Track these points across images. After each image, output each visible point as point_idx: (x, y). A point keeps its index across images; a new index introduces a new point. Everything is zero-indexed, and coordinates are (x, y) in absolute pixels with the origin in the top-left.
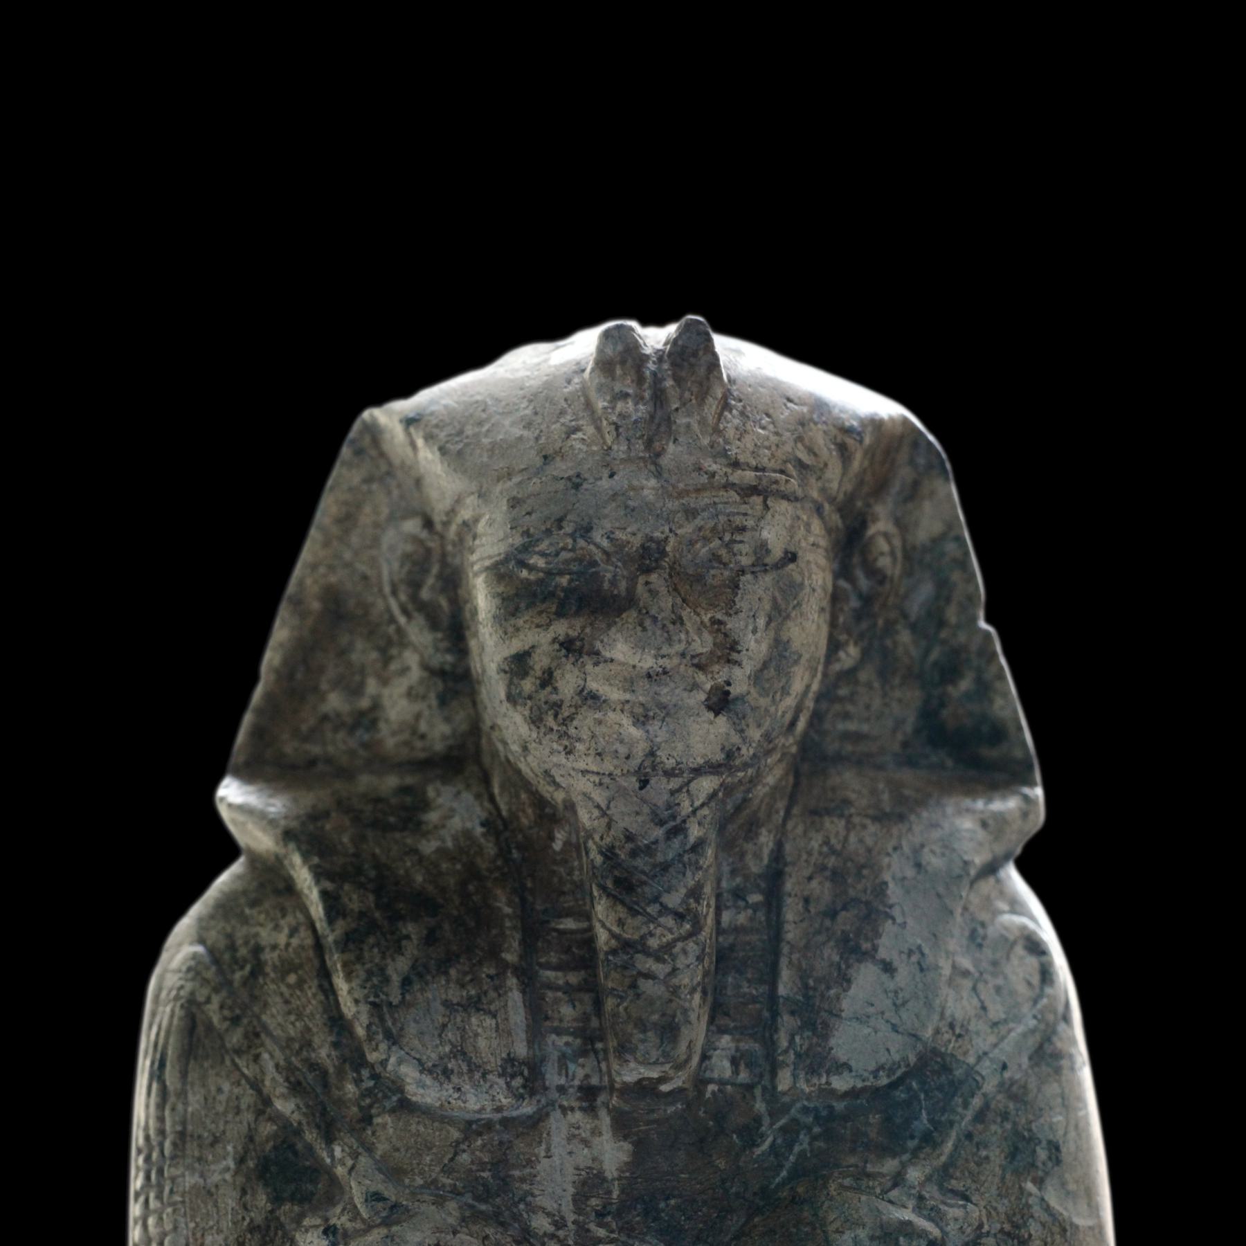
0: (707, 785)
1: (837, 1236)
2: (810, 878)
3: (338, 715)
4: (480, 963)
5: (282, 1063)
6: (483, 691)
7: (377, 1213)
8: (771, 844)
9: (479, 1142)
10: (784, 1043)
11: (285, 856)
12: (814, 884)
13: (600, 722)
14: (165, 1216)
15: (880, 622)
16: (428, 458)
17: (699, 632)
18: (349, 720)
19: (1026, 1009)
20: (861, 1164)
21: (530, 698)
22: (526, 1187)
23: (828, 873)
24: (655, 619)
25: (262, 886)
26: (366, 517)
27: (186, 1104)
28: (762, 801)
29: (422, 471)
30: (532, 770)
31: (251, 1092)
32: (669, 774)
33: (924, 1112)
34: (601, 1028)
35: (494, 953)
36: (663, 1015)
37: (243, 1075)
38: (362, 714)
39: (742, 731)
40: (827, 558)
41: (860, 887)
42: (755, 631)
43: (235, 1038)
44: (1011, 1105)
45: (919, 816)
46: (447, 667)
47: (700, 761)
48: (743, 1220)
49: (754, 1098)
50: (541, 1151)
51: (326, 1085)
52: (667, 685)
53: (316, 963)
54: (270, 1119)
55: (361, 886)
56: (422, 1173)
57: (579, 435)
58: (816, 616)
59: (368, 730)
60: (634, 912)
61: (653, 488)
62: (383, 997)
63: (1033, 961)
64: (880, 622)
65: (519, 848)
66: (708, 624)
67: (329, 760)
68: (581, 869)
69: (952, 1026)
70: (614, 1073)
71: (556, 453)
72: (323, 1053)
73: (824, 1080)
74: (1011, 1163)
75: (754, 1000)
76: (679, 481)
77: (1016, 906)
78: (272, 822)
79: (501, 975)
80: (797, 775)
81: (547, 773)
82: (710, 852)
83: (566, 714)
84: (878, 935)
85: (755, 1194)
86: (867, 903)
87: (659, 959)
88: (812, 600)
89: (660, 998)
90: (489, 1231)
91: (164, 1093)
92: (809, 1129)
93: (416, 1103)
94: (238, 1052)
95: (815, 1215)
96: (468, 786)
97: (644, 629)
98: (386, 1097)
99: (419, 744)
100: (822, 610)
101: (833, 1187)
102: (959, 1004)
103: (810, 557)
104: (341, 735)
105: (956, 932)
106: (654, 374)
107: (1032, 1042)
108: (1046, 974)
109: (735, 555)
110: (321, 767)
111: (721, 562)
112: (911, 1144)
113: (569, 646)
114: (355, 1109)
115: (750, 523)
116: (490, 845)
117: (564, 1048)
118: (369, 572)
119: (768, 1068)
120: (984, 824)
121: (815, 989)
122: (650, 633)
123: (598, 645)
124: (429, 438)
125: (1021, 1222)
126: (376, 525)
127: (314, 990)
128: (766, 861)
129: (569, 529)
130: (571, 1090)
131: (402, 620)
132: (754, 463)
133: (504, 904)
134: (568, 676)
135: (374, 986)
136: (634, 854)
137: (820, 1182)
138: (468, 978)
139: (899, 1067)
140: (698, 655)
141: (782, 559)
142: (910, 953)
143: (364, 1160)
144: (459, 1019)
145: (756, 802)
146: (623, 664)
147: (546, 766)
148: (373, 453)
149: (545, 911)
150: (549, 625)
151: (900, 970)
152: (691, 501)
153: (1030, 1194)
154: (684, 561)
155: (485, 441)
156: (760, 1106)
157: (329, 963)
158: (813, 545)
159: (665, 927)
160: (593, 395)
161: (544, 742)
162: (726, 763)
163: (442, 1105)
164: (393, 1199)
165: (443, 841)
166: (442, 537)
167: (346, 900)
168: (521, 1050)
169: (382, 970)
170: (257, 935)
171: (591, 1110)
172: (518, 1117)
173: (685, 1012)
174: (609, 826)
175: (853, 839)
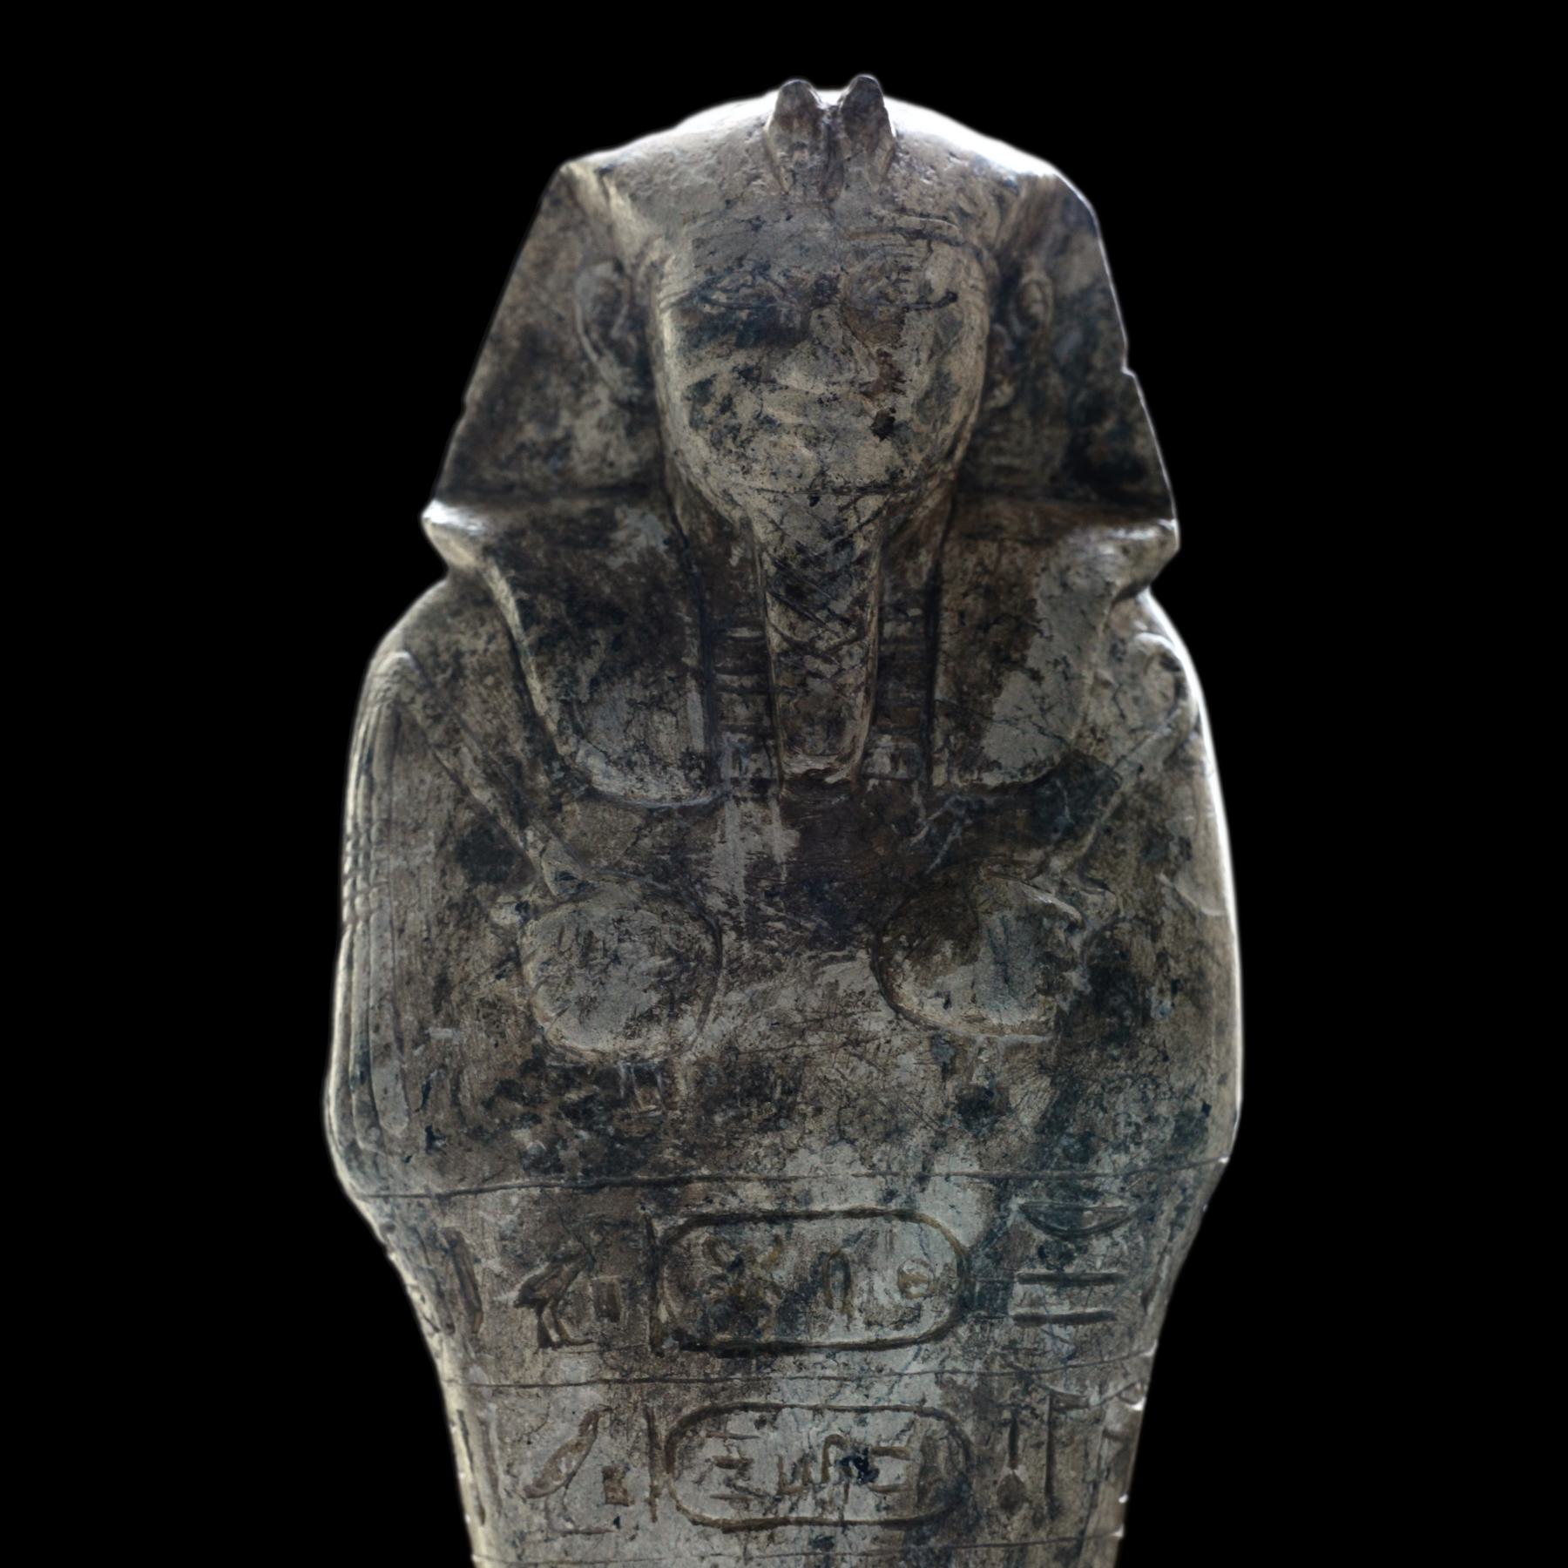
0: (872, 503)
1: (986, 916)
2: (965, 595)
3: (534, 444)
4: (662, 667)
5: (480, 757)
6: (668, 418)
7: (565, 891)
8: (930, 564)
9: (659, 829)
10: (939, 743)
11: (485, 570)
12: (969, 600)
13: (775, 445)
14: (370, 896)
15: (1033, 365)
16: (619, 205)
17: (867, 362)
18: (544, 450)
19: (1161, 718)
20: (1008, 853)
21: (711, 422)
22: (702, 869)
23: (981, 591)
24: (826, 349)
25: (463, 597)
26: (562, 262)
27: (391, 794)
28: (922, 522)
29: (614, 217)
30: (711, 490)
31: (451, 782)
32: (838, 492)
33: (1067, 810)
34: (773, 727)
35: (675, 658)
36: (830, 710)
37: (445, 768)
38: (556, 443)
39: (905, 455)
40: (985, 300)
41: (1011, 603)
42: (918, 363)
43: (437, 735)
44: (1147, 805)
45: (1066, 543)
46: (635, 400)
47: (867, 481)
48: (900, 902)
49: (912, 793)
50: (716, 837)
51: (520, 776)
52: (837, 410)
53: (512, 666)
54: (469, 807)
55: (553, 596)
56: (607, 855)
57: (759, 182)
58: (974, 353)
59: (561, 458)
60: (803, 617)
61: (826, 231)
62: (574, 696)
63: (1167, 676)
64: (1033, 365)
65: (698, 563)
66: (875, 355)
67: (525, 486)
68: (755, 582)
69: (1093, 731)
70: (784, 765)
71: (737, 198)
72: (518, 747)
73: (975, 777)
74: (1146, 856)
75: (912, 703)
76: (849, 224)
77: (1152, 627)
78: (473, 539)
80: (954, 503)
81: (725, 492)
82: (874, 565)
83: (744, 437)
84: (1027, 646)
85: (911, 878)
86: (1017, 618)
87: (827, 660)
88: (971, 338)
89: (827, 695)
91: (371, 786)
92: (962, 821)
93: (602, 792)
94: (439, 746)
95: (966, 897)
96: (652, 509)
97: (817, 358)
98: (575, 787)
99: (607, 471)
100: (980, 347)
101: (982, 872)
102: (1101, 712)
103: (970, 298)
104: (536, 463)
105: (1099, 646)
106: (829, 127)
107: (1167, 748)
108: (1180, 689)
109: (901, 293)
110: (517, 492)
111: (888, 300)
112: (1055, 837)
113: (748, 376)
114: (546, 798)
115: (915, 264)
116: (672, 561)
118: (563, 313)
119: (924, 765)
120: (1125, 551)
121: (968, 694)
122: (822, 362)
123: (774, 374)
124: (621, 186)
125: (1154, 909)
126: (571, 270)
127: (510, 691)
128: (925, 578)
129: (748, 266)
130: (744, 783)
131: (594, 357)
132: (919, 209)
133: (684, 614)
134: (746, 402)
135: (565, 686)
136: (805, 564)
137: (972, 868)
138: (651, 679)
139: (1045, 766)
140: (866, 384)
141: (944, 298)
142: (1056, 663)
143: (554, 844)
144: (642, 716)
145: (917, 524)
146: (797, 391)
147: (725, 486)
148: (569, 203)
149: (723, 621)
150: (729, 355)
151: (1047, 678)
152: (861, 242)
153: (1163, 885)
154: (854, 298)
155: (673, 188)
156: (917, 800)
157: (524, 666)
158: (973, 287)
159: (833, 632)
160: (772, 145)
161: (724, 463)
162: (889, 484)
163: (625, 795)
164: (580, 878)
165: (630, 557)
166: (631, 280)
167: (539, 608)
168: (699, 745)
169: (572, 672)
170: (457, 642)
171: (762, 801)
172: (695, 806)
173: (850, 708)
174: (782, 539)
175: (1005, 560)
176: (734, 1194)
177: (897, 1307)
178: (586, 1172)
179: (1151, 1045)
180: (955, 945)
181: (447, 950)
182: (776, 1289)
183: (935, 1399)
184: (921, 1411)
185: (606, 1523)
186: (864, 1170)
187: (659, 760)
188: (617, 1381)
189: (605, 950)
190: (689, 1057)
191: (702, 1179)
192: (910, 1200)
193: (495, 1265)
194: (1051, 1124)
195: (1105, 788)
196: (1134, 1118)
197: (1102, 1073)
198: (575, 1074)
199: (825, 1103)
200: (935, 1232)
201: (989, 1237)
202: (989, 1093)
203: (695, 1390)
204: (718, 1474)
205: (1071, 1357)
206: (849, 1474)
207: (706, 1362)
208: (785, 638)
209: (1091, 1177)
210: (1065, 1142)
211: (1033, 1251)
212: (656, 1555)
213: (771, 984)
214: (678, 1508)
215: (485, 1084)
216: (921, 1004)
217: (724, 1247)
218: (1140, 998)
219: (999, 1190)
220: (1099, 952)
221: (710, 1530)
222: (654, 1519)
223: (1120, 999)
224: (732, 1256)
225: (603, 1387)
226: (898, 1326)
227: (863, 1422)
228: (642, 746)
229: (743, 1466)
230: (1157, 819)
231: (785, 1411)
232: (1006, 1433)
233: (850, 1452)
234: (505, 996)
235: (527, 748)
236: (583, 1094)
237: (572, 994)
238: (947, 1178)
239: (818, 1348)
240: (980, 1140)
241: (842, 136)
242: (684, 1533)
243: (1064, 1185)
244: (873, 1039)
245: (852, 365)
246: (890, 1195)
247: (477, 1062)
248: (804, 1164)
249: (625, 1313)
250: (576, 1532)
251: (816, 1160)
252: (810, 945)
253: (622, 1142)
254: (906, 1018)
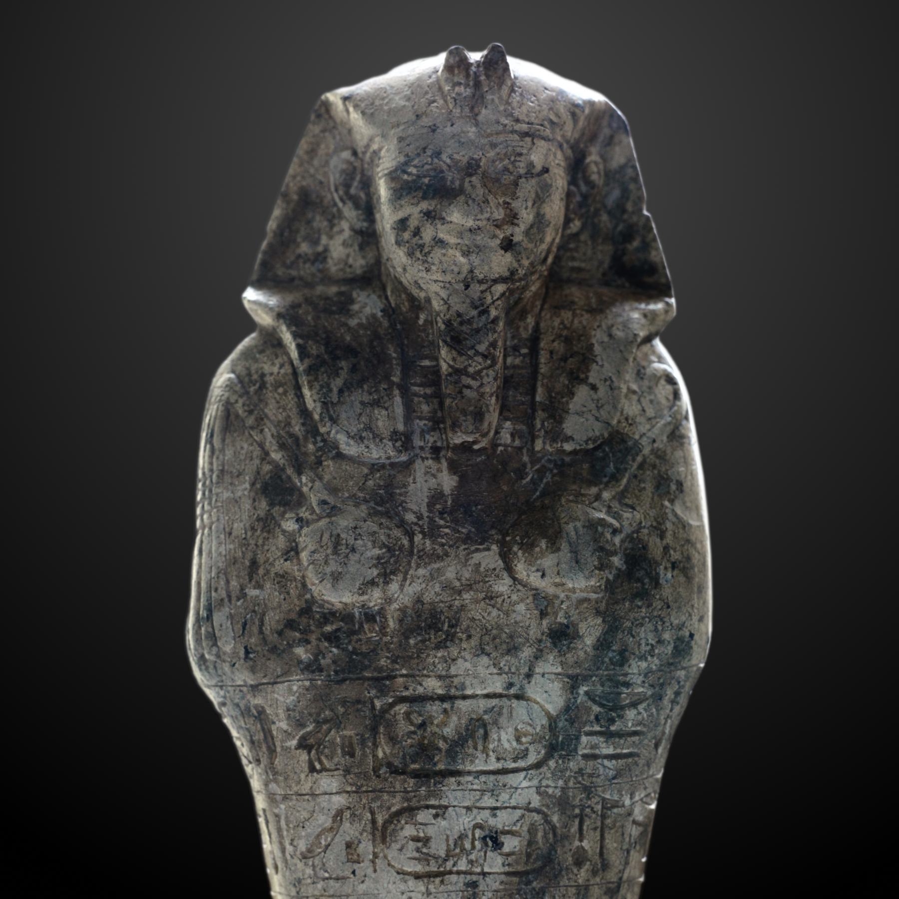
0: (500, 288)
1: (565, 525)
2: (553, 341)
3: (306, 255)
4: (380, 382)
5: (275, 434)
6: (383, 240)
7: (324, 511)
8: (533, 323)
9: (378, 475)
10: (539, 426)
11: (278, 327)
12: (556, 344)
13: (444, 255)
14: (212, 514)
15: (592, 209)
16: (355, 118)
17: (497, 207)
18: (312, 258)
19: (666, 412)
20: (578, 489)
21: (408, 242)
22: (402, 498)
23: (563, 339)
24: (474, 200)
25: (265, 342)
26: (322, 150)
27: (224, 455)
28: (529, 299)
29: (352, 124)
30: (408, 281)
31: (259, 449)
32: (481, 282)
33: (612, 464)
34: (443, 417)
35: (387, 377)
36: (476, 407)
37: (255, 440)
38: (319, 254)
39: (519, 261)
40: (565, 172)
41: (579, 346)
42: (526, 208)
43: (250, 421)
44: (658, 461)
45: (611, 311)
46: (364, 229)
47: (497, 276)
48: (516, 517)
49: (523, 455)
50: (411, 480)
51: (298, 445)
52: (480, 235)
53: (294, 382)
54: (269, 463)
55: (317, 342)
56: (348, 490)
57: (435, 104)
58: (559, 202)
59: (321, 263)
60: (460, 354)
61: (474, 132)
62: (329, 399)
63: (669, 388)
64: (592, 209)
65: (400, 323)
66: (502, 204)
67: (301, 278)
68: (433, 334)
69: (627, 419)
70: (449, 439)
71: (423, 113)
72: (297, 428)
73: (559, 445)
74: (657, 491)
75: (523, 403)
76: (487, 129)
77: (661, 359)
78: (271, 309)
80: (547, 288)
81: (416, 282)
82: (501, 324)
83: (427, 251)
84: (589, 371)
85: (522, 504)
86: (583, 354)
87: (474, 379)
88: (557, 194)
89: (474, 398)
90: (383, 521)
91: (213, 451)
92: (551, 471)
93: (345, 454)
94: (252, 428)
95: (554, 514)
96: (374, 292)
97: (468, 205)
98: (329, 451)
99: (348, 270)
100: (562, 199)
101: (563, 500)
102: (631, 408)
103: (556, 171)
104: (307, 265)
105: (630, 370)
106: (475, 73)
107: (669, 429)
108: (676, 395)
109: (516, 168)
110: (297, 282)
111: (509, 172)
112: (605, 480)
113: (429, 215)
114: (313, 457)
115: (525, 151)
116: (385, 321)
117: (423, 427)
118: (323, 180)
119: (530, 439)
120: (645, 316)
121: (555, 398)
122: (471, 208)
123: (444, 214)
124: (356, 106)
125: (662, 521)
126: (327, 155)
127: (292, 396)
128: (530, 331)
129: (429, 153)
130: (427, 449)
131: (340, 205)
132: (527, 120)
133: (392, 352)
134: (428, 230)
135: (324, 393)
136: (461, 323)
137: (557, 498)
138: (373, 390)
139: (599, 439)
140: (496, 220)
141: (541, 171)
142: (606, 380)
143: (318, 484)
144: (368, 411)
145: (526, 300)
146: (457, 224)
147: (416, 278)
148: (326, 116)
149: (414, 356)
150: (418, 204)
151: (600, 389)
152: (494, 139)
153: (667, 507)
154: (490, 171)
155: (386, 108)
156: (525, 458)
157: (300, 382)
158: (558, 164)
159: (477, 362)
160: (443, 83)
161: (415, 265)
162: (510, 278)
163: (359, 456)
164: (333, 503)
165: (361, 319)
166: (362, 160)
167: (309, 349)
168: (401, 427)
169: (328, 385)
170: (262, 368)
171: (437, 459)
172: (398, 462)
173: (487, 406)
174: (448, 309)
175: (576, 321)
176: (421, 685)
177: (515, 749)
178: (336, 672)
179: (660, 599)
180: (548, 542)
181: (256, 545)
182: (445, 739)
183: (536, 802)
184: (528, 809)
185: (348, 873)
186: (495, 671)
187: (378, 436)
188: (354, 792)
189: (347, 545)
191: (402, 676)
192: (522, 688)
193: (284, 725)
194: (602, 645)
195: (633, 452)
196: (650, 641)
197: (632, 615)
198: (330, 616)
199: (473, 632)
200: (536, 706)
201: (567, 709)
202: (567, 627)
203: (398, 797)
204: (412, 845)
205: (614, 778)
206: (487, 845)
207: (405, 781)
208: (450, 366)
209: (626, 675)
210: (610, 654)
211: (592, 717)
212: (376, 892)
213: (442, 564)
214: (389, 865)
215: (278, 621)
216: (528, 575)
217: (415, 715)
218: (654, 572)
219: (573, 682)
220: (630, 546)
221: (407, 877)
222: (375, 871)
223: (642, 573)
224: (420, 720)
225: (345, 795)
226: (515, 760)
227: (495, 816)
228: (368, 428)
229: (426, 841)
230: (664, 469)
231: (450, 809)
232: (577, 821)
233: (487, 832)
234: (289, 571)
235: (302, 429)
236: (334, 627)
237: (328, 570)
238: (543, 675)
239: (469, 773)
240: (562, 654)
241: (483, 78)
242: (392, 879)
243: (610, 679)
244: (501, 596)
245: (489, 209)
246: (511, 685)
247: (273, 609)
248: (461, 667)
249: (358, 753)
250: (330, 878)
251: (468, 665)
252: (464, 542)
253: (357, 655)
254: (519, 584)
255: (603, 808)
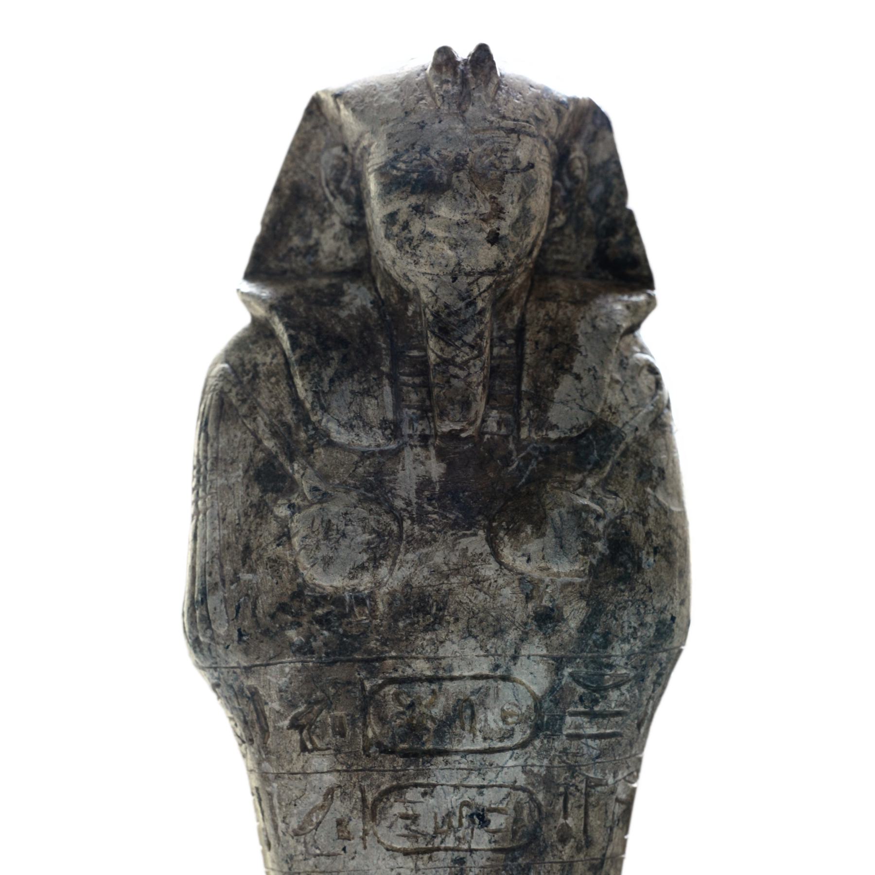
0: (487, 281)
1: (550, 511)
2: (539, 332)
3: (298, 248)
4: (370, 372)
5: (268, 422)
6: (373, 233)
7: (316, 497)
8: (519, 315)
9: (368, 462)
10: (524, 415)
11: (270, 318)
12: (541, 335)
13: (432, 248)
14: (207, 500)
15: (576, 203)
16: (346, 114)
17: (484, 202)
18: (304, 251)
19: (648, 401)
20: (562, 476)
21: (397, 236)
22: (392, 485)
23: (548, 330)
24: (461, 195)
25: (258, 333)
26: (313, 146)
27: (218, 443)
28: (514, 291)
29: (343, 121)
30: (397, 274)
31: (252, 437)
32: (468, 274)
33: (595, 452)
34: (431, 406)
35: (377, 367)
36: (463, 396)
37: (248, 428)
38: (310, 247)
39: (505, 254)
40: (549, 167)
41: (564, 336)
42: (512, 203)
43: (244, 410)
44: (640, 449)
45: (595, 303)
46: (354, 223)
47: (484, 268)
48: (502, 504)
49: (509, 443)
50: (400, 467)
51: (290, 433)
52: (467, 229)
53: (286, 372)
54: (262, 450)
55: (309, 332)
56: (339, 477)
57: (424, 101)
58: (544, 197)
59: (313, 256)
60: (448, 344)
61: (461, 129)
62: (320, 388)
63: (651, 377)
64: (576, 203)
65: (390, 314)
66: (488, 198)
67: (293, 271)
68: (422, 325)
69: (610, 408)
70: (437, 427)
71: (411, 110)
72: (289, 417)
73: (544, 433)
74: (639, 478)
75: (509, 393)
76: (474, 125)
78: (264, 301)
79: (379, 380)
80: (533, 281)
81: (405, 275)
82: (488, 315)
83: (415, 244)
84: (573, 361)
85: (508, 490)
86: (568, 345)
87: (461, 368)
88: (542, 188)
89: (462, 388)
90: (373, 507)
92: (537, 458)
93: (336, 442)
94: (245, 416)
95: (539, 501)
96: (364, 284)
97: (456, 200)
98: (321, 439)
99: (339, 263)
100: (547, 194)
101: (548, 487)
102: (614, 397)
103: (541, 166)
104: (299, 258)
105: (613, 360)
106: (462, 71)
107: (651, 418)
109: (503, 163)
110: (289, 275)
111: (495, 167)
112: (589, 467)
113: (418, 210)
114: (305, 445)
115: (511, 147)
116: (375, 313)
117: (412, 416)
118: (314, 175)
119: (516, 427)
120: (628, 307)
121: (540, 387)
122: (459, 202)
123: (432, 209)
124: (346, 104)
125: (644, 507)
126: (319, 150)
127: (284, 385)
128: (516, 322)
129: (417, 148)
130: (415, 437)
131: (331, 199)
132: (513, 117)
133: (382, 343)
134: (417, 224)
135: (315, 383)
136: (449, 315)
137: (542, 484)
138: (363, 379)
139: (583, 427)
140: (483, 214)
141: (527, 166)
142: (589, 370)
143: (309, 471)
144: (358, 400)
145: (512, 292)
146: (445, 218)
147: (405, 271)
148: (318, 113)
149: (403, 347)
150: (407, 198)
151: (584, 379)
152: (481, 135)
153: (649, 494)
154: (477, 166)
155: (375, 105)
156: (511, 446)
157: (292, 372)
158: (543, 160)
159: (465, 353)
160: (431, 81)
161: (404, 258)
162: (496, 270)
163: (349, 443)
164: (324, 490)
165: (351, 311)
166: (352, 156)
167: (301, 339)
168: (390, 416)
169: (319, 375)
170: (255, 358)
171: (425, 447)
172: (388, 450)
173: (474, 395)
174: (436, 301)
175: (561, 313)
176: (410, 666)
177: (501, 729)
178: (327, 654)
179: (642, 583)
180: (533, 527)
181: (249, 530)
182: (433, 719)
183: (522, 781)
184: (514, 787)
185: (338, 850)
186: (482, 653)
187: (368, 424)
188: (345, 771)
189: (338, 530)
190: (385, 590)
191: (392, 658)
192: (508, 669)
193: (276, 706)
194: (586, 627)
195: (616, 440)
196: (633, 624)
197: (615, 599)
198: (321, 599)
199: (460, 615)
200: (522, 687)
201: (552, 690)
202: (552, 610)
203: (388, 776)
204: (401, 823)
205: (597, 757)
206: (474, 822)
207: (394, 760)
208: (438, 356)
209: (609, 657)
210: (594, 637)
211: (577, 698)
212: (366, 868)
213: (430, 549)
214: (379, 842)
215: (271, 605)
216: (514, 560)
217: (404, 696)
218: (636, 557)
219: (558, 664)
220: (613, 531)
221: (396, 854)
222: (365, 848)
223: (625, 557)
224: (408, 701)
225: (336, 774)
226: (501, 740)
227: (481, 794)
228: (358, 416)
229: (415, 818)
230: (646, 457)
231: (438, 787)
232: (561, 799)
233: (474, 810)
234: (282, 556)
235: (294, 417)
236: (325, 610)
237: (319, 555)
238: (529, 657)
239: (457, 752)
240: (547, 636)
241: (470, 76)
242: (382, 855)
243: (594, 661)
244: (487, 580)
245: (476, 204)
246: (497, 667)
247: (266, 593)
248: (449, 649)
249: (349, 733)
250: (322, 855)
251: (455, 647)
252: (452, 527)
253: (347, 637)
254: (505, 568)
255: (587, 786)
